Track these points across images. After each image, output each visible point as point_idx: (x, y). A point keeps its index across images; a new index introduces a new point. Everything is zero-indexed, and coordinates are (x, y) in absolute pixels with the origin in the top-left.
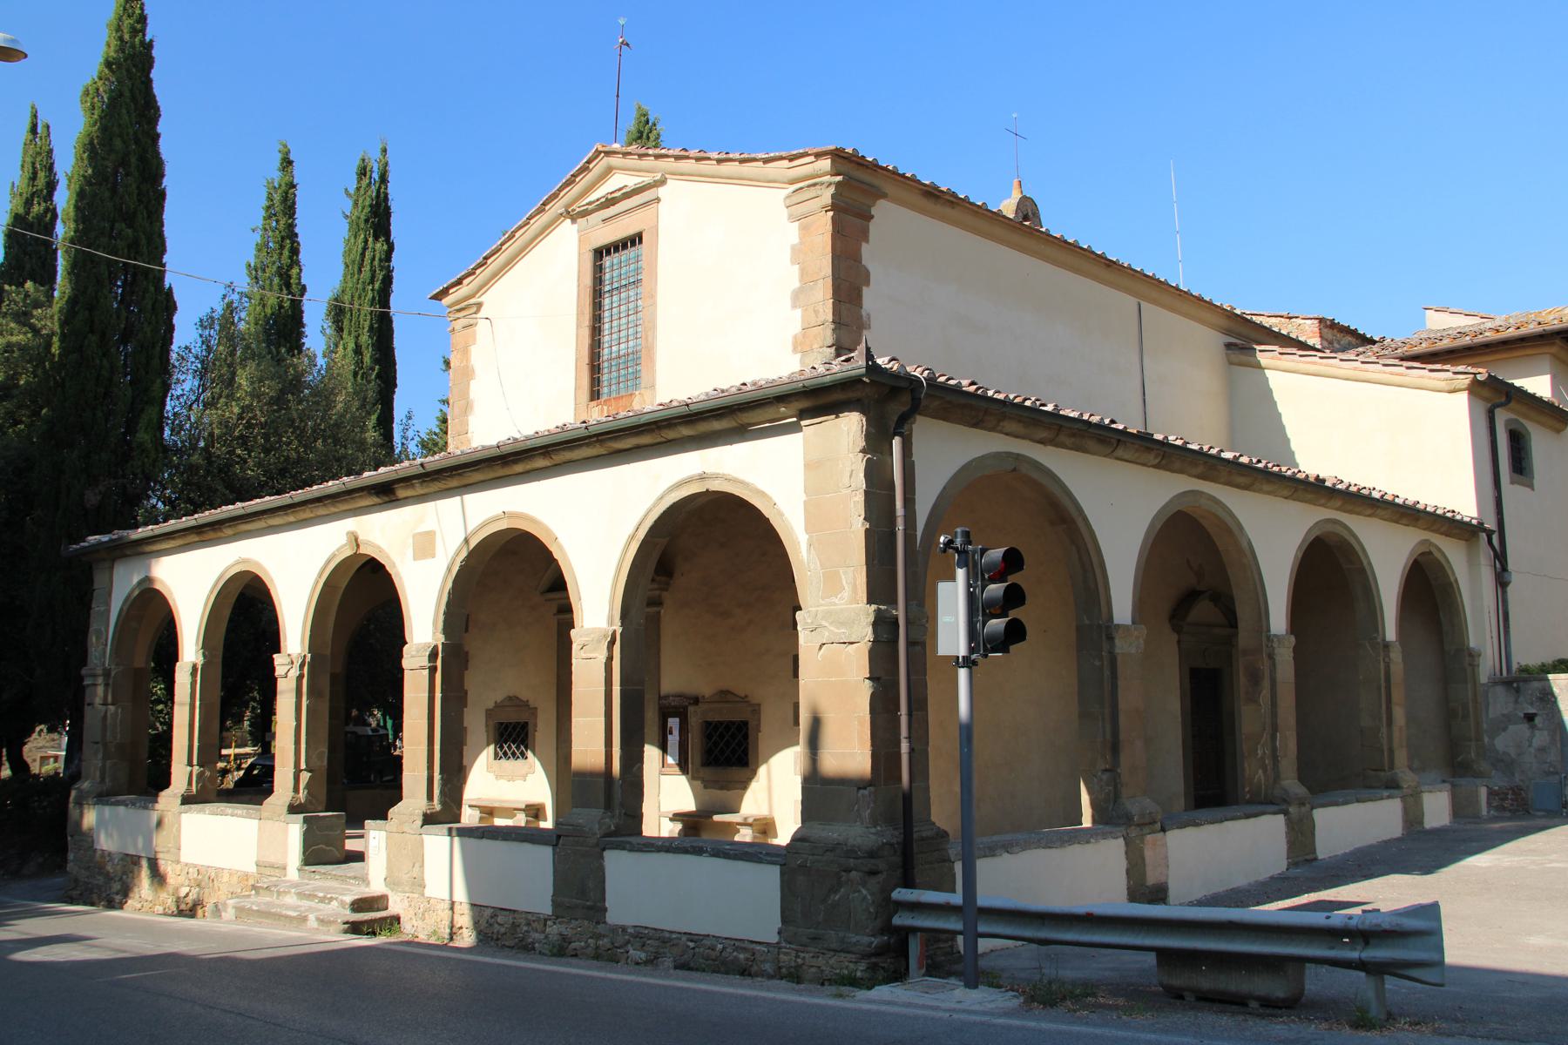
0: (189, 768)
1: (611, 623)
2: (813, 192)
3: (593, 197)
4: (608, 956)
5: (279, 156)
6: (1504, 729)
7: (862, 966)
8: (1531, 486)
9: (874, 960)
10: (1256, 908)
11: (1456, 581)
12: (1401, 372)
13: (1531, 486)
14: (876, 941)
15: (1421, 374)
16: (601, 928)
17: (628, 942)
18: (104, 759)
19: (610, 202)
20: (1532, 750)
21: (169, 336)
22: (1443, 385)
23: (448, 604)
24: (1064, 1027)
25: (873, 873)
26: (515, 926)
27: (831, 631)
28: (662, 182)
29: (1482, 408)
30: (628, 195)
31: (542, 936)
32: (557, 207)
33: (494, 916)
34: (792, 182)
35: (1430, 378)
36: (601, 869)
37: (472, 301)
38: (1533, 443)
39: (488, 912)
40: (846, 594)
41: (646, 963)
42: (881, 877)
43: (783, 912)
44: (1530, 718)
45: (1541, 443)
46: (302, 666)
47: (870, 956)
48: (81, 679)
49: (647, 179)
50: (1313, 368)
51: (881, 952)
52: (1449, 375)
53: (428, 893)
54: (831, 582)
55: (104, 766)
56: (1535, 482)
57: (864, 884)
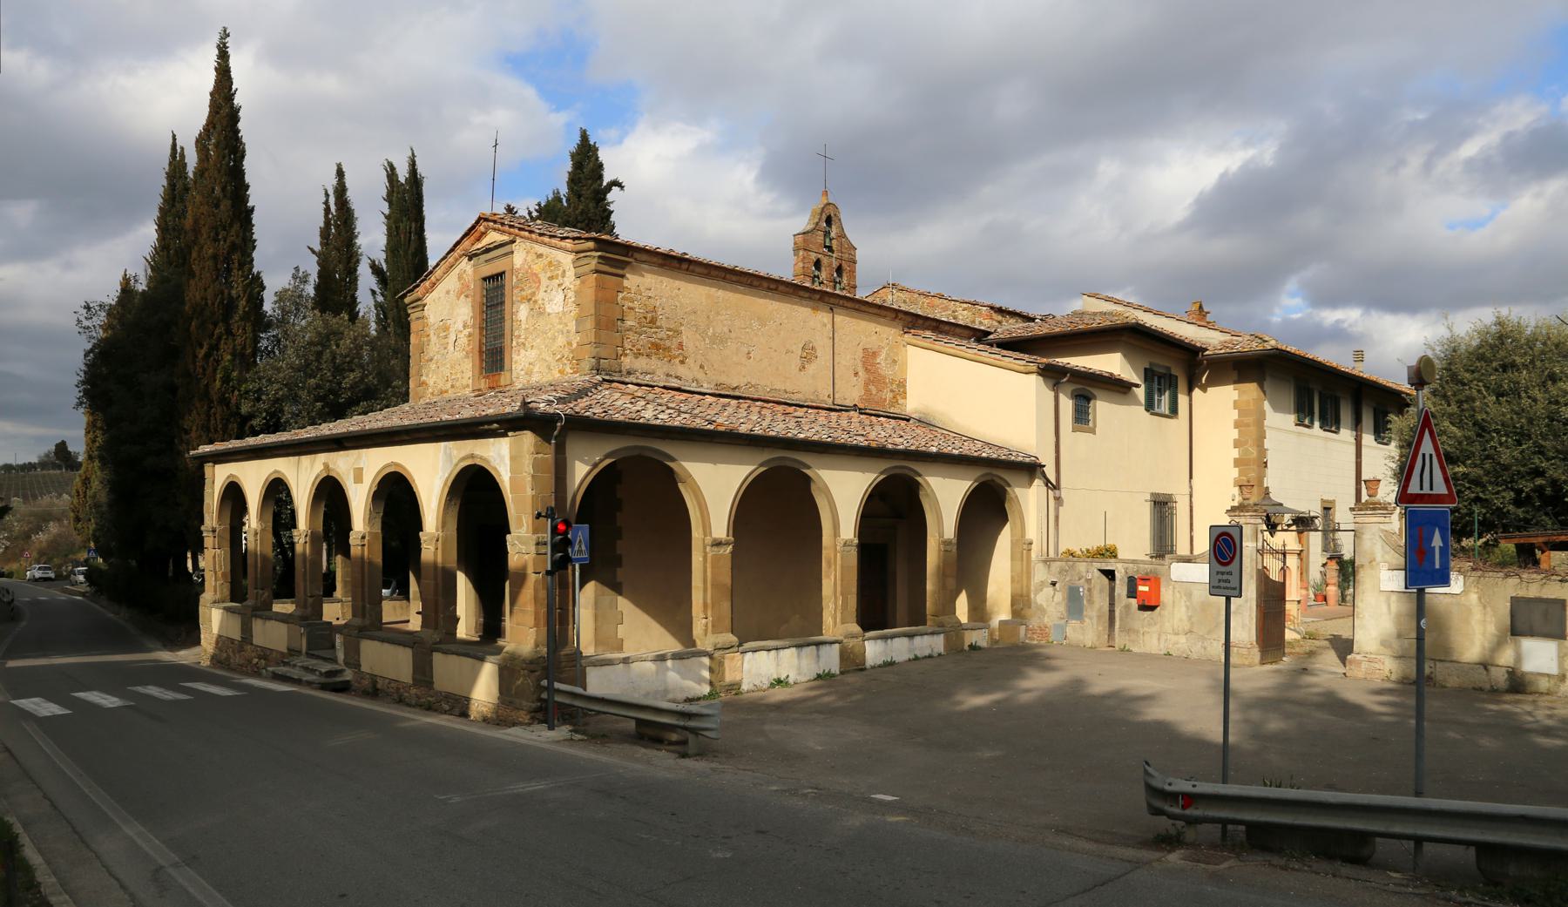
1: (437, 530)
2: (586, 261)
3: (479, 245)
4: (429, 708)
5: (336, 168)
6: (1041, 590)
7: (528, 717)
8: (1093, 431)
9: (533, 714)
12: (998, 355)
14: (534, 705)
15: (1010, 358)
16: (431, 692)
17: (441, 700)
18: (216, 580)
19: (488, 250)
20: (1053, 604)
22: (1022, 368)
25: (533, 672)
26: (398, 689)
28: (513, 242)
30: (496, 247)
32: (459, 251)
33: (389, 683)
34: (577, 253)
35: (1015, 364)
36: (431, 661)
37: (419, 303)
39: (387, 681)
40: (525, 528)
42: (537, 674)
44: (1054, 584)
47: (531, 712)
48: (202, 533)
49: (506, 238)
50: (952, 351)
51: (537, 710)
52: (1024, 363)
55: (216, 585)
57: (529, 676)
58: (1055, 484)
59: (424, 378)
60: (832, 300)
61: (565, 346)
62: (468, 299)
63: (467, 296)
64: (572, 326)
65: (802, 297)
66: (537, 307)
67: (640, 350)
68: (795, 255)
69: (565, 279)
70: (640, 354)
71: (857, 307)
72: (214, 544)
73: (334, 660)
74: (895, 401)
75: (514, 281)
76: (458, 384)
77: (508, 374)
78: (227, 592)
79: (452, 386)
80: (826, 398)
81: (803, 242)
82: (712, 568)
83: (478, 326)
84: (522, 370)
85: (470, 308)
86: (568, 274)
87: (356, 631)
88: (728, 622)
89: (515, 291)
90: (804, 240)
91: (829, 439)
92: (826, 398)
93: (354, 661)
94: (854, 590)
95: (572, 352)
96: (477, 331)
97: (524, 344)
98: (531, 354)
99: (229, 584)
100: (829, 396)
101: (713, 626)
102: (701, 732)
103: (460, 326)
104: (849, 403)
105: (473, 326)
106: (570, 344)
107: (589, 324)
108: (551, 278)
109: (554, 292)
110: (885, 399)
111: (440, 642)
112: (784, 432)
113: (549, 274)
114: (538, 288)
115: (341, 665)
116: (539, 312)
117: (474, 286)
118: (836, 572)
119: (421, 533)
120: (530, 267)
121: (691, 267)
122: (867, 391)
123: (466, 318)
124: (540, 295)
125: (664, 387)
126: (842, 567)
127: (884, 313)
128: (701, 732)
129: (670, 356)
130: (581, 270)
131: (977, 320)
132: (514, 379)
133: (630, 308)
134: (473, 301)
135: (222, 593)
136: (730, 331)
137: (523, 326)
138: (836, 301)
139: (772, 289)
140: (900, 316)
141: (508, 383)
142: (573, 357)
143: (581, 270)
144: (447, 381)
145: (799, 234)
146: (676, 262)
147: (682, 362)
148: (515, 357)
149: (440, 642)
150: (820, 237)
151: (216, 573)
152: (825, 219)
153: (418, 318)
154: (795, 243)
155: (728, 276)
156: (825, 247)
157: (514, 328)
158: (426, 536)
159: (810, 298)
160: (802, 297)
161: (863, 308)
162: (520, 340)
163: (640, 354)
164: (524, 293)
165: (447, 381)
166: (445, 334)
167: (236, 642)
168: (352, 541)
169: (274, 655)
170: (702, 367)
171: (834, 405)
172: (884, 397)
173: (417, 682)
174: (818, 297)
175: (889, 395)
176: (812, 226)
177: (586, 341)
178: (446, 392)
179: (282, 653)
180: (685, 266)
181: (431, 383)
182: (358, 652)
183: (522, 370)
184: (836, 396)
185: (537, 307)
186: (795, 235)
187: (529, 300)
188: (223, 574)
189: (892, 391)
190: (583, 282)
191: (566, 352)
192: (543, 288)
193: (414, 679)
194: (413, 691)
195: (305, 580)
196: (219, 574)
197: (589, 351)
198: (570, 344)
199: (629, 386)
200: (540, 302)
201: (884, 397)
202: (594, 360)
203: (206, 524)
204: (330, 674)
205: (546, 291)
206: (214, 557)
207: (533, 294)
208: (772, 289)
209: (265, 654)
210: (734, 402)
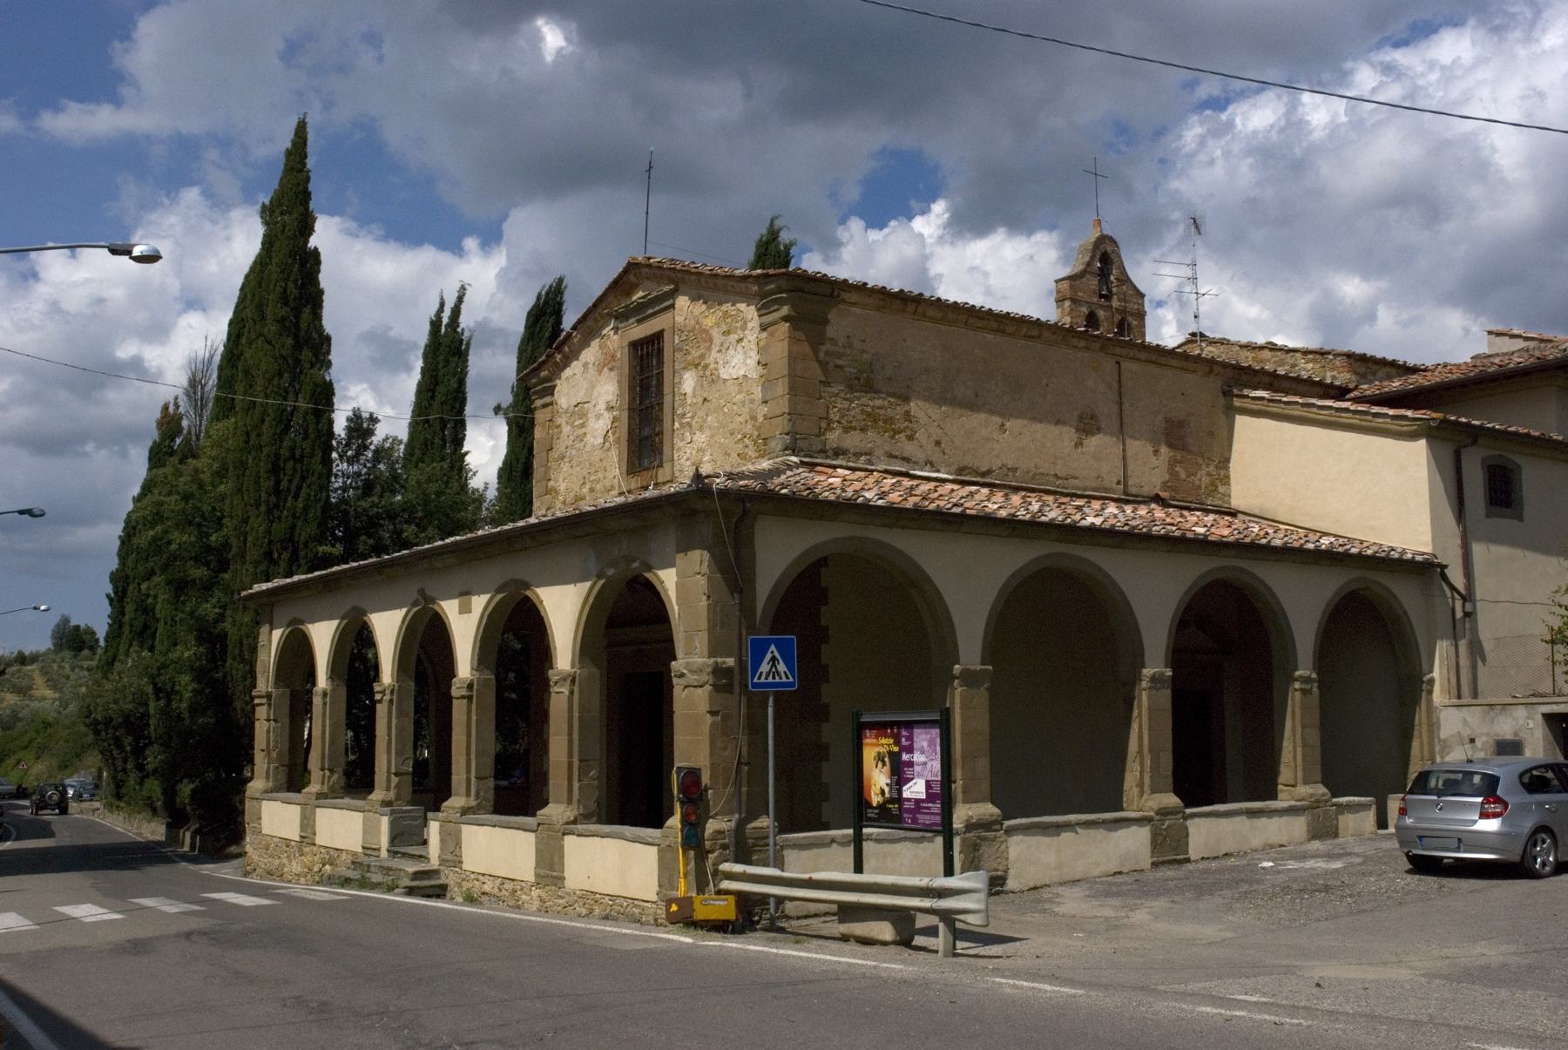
0: (321, 773)
1: (573, 666)
8: (1521, 519)
10: (15, 802)
11: (1405, 613)
13: (1521, 519)
18: (269, 763)
21: (130, 563)
23: (546, 630)
24: (766, 949)
27: (692, 678)
29: (1447, 452)
31: (529, 898)
36: (562, 848)
38: (1524, 477)
41: (586, 915)
43: (659, 882)
45: (1534, 477)
46: (392, 692)
53: (465, 866)
54: (689, 639)
56: (1525, 513)
58: (1463, 592)
59: (551, 483)
60: (1118, 351)
61: (746, 422)
62: (613, 373)
63: (611, 369)
64: (758, 394)
65: (1076, 347)
66: (708, 373)
67: (851, 422)
68: (1058, 308)
69: (747, 332)
70: (851, 428)
71: (1154, 358)
72: (268, 714)
73: (423, 858)
74: (1213, 489)
75: (676, 342)
76: (598, 487)
77: (667, 466)
78: (283, 778)
79: (592, 490)
80: (1114, 485)
81: (1069, 290)
82: (962, 708)
83: (627, 406)
84: (688, 459)
85: (616, 385)
86: (750, 325)
87: (458, 815)
88: (985, 786)
89: (677, 355)
90: (1071, 287)
91: (1126, 528)
92: (1114, 485)
93: (453, 856)
94: (1169, 745)
95: (758, 429)
96: (626, 414)
97: (689, 424)
98: (701, 438)
99: (286, 769)
100: (1118, 483)
101: (964, 792)
102: (958, 917)
103: (602, 406)
104: (1147, 490)
105: (620, 409)
106: (753, 418)
107: (781, 388)
108: (727, 333)
109: (731, 351)
110: (1200, 486)
111: (575, 822)
112: (1060, 518)
113: (724, 328)
114: (709, 349)
115: (434, 862)
116: (710, 378)
117: (623, 355)
118: (1141, 719)
119: (550, 672)
120: (697, 323)
121: (920, 310)
122: (1173, 474)
123: (610, 397)
124: (710, 360)
125: (886, 471)
126: (1150, 709)
127: (1191, 366)
128: (958, 917)
129: (893, 430)
130: (769, 318)
131: (1329, 374)
132: (677, 474)
133: (837, 366)
134: (620, 375)
135: (276, 780)
136: (977, 395)
137: (689, 401)
138: (1124, 352)
139: (1033, 337)
140: (1217, 369)
141: (669, 478)
142: (759, 435)
143: (769, 318)
144: (584, 483)
145: (1063, 279)
146: (898, 302)
147: (910, 438)
148: (678, 443)
149: (575, 822)
150: (1093, 283)
151: (269, 752)
152: (1098, 257)
153: (545, 406)
154: (1058, 292)
155: (971, 321)
156: (1101, 296)
157: (676, 405)
158: (557, 675)
159: (1087, 348)
160: (1076, 347)
161: (1163, 360)
162: (685, 421)
163: (851, 428)
164: (689, 358)
165: (584, 483)
166: (581, 421)
167: (293, 844)
168: (455, 692)
169: (344, 856)
170: (938, 443)
171: (1128, 495)
172: (1197, 483)
173: (541, 880)
174: (1098, 346)
175: (1206, 480)
176: (1080, 268)
177: (779, 412)
178: (583, 498)
179: (355, 854)
180: (911, 307)
181: (562, 487)
182: (458, 844)
183: (688, 459)
184: (1130, 482)
185: (708, 373)
186: (1057, 281)
187: (696, 366)
188: (279, 754)
189: (1209, 474)
190: (771, 335)
191: (749, 428)
192: (715, 349)
193: (537, 875)
194: (535, 893)
195: (389, 752)
196: (274, 754)
197: (782, 424)
198: (753, 418)
199: (839, 470)
200: (712, 366)
201: (1197, 483)
202: (788, 437)
203: (258, 689)
204: (418, 875)
205: (720, 351)
206: (268, 731)
207: (702, 357)
208: (1033, 337)
209: (331, 856)
210: (985, 491)
